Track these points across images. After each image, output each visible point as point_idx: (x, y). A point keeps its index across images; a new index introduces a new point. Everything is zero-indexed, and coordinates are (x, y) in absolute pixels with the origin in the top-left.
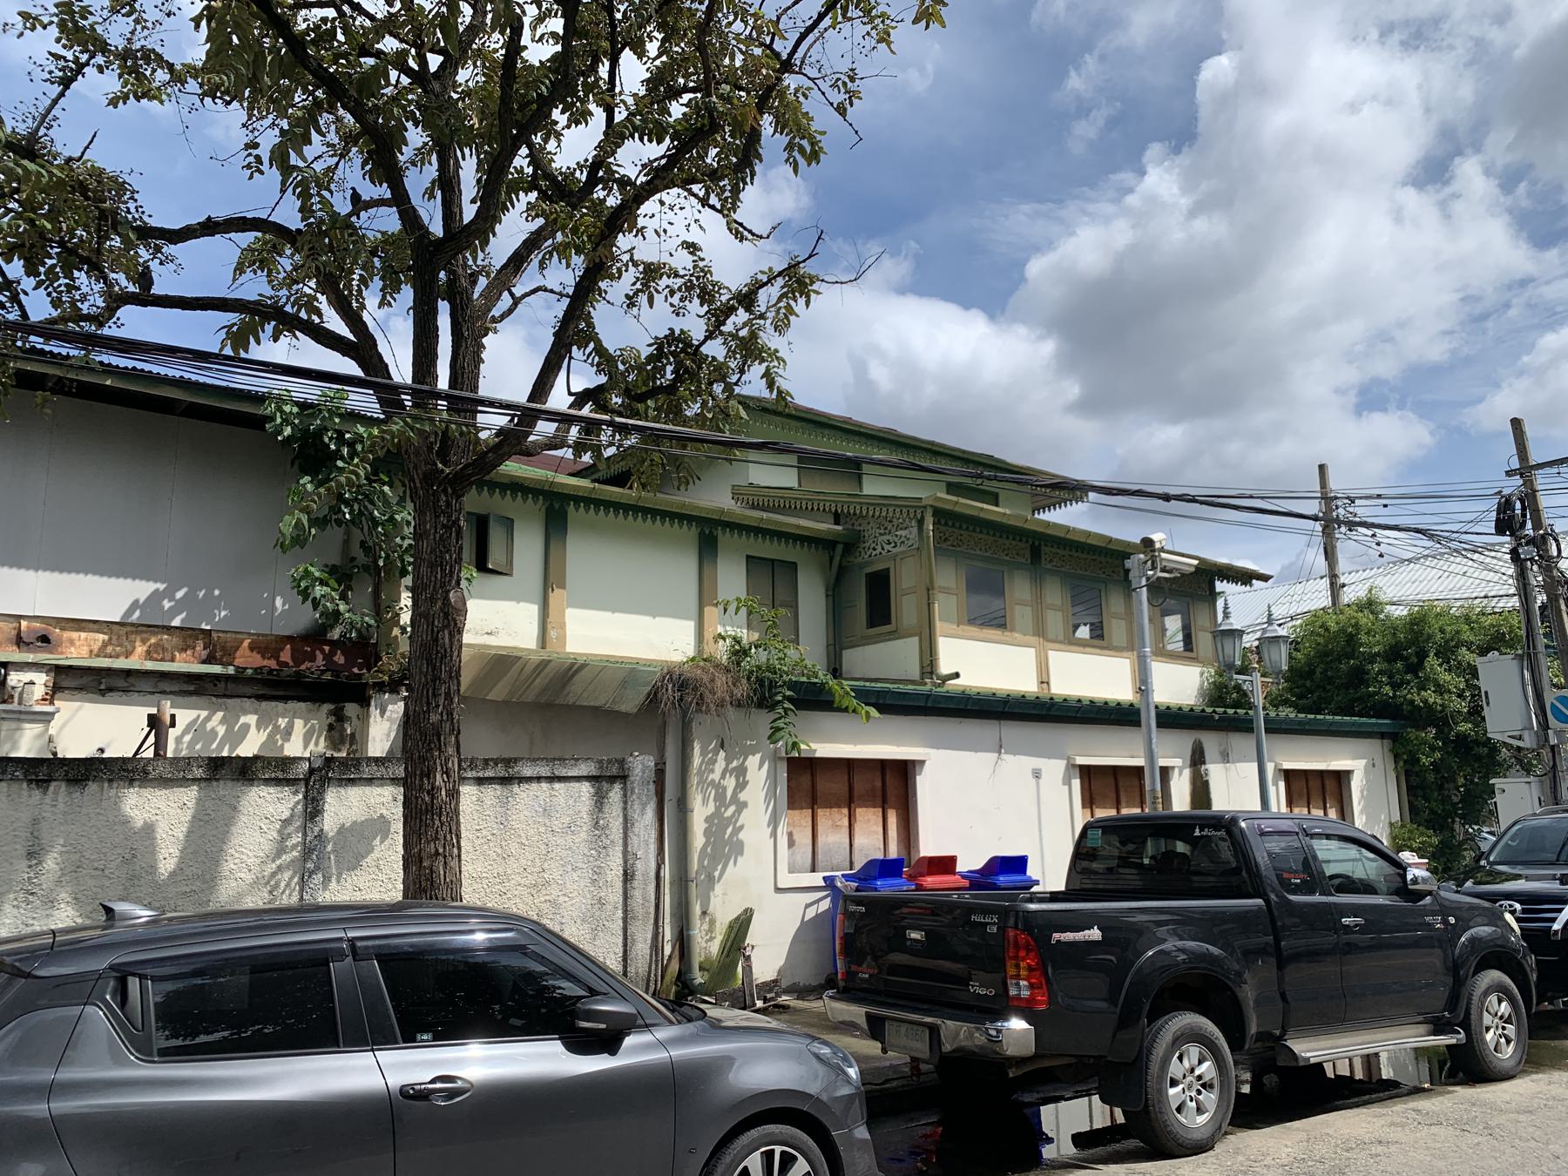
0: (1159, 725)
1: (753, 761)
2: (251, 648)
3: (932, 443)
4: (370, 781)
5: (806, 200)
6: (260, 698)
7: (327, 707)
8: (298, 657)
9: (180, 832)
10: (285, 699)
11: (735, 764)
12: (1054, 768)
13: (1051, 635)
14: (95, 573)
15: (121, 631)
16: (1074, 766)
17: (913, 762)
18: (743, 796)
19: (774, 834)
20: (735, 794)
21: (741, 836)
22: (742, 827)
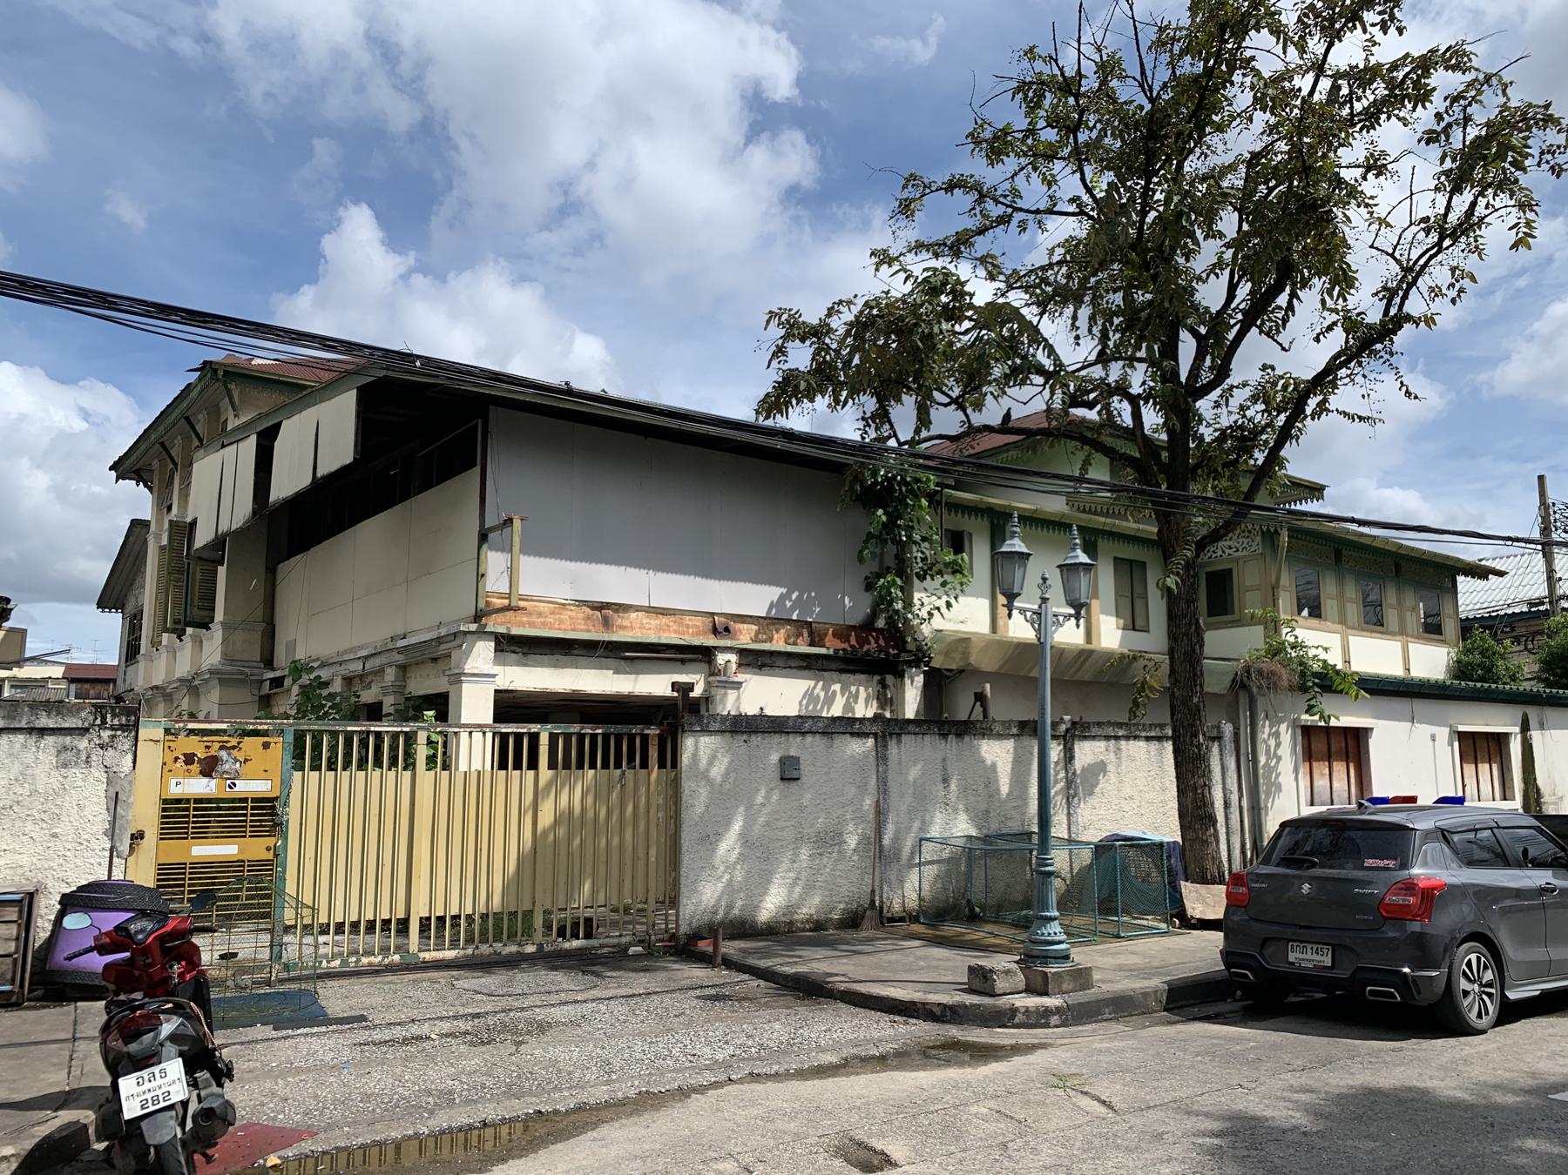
1: (1283, 727)
2: (834, 635)
4: (1094, 738)
5: (811, 165)
6: (842, 671)
7: (877, 678)
8: (863, 641)
9: (1008, 768)
10: (853, 672)
12: (1443, 733)
13: (1350, 623)
14: (697, 574)
15: (768, 623)
19: (1296, 779)
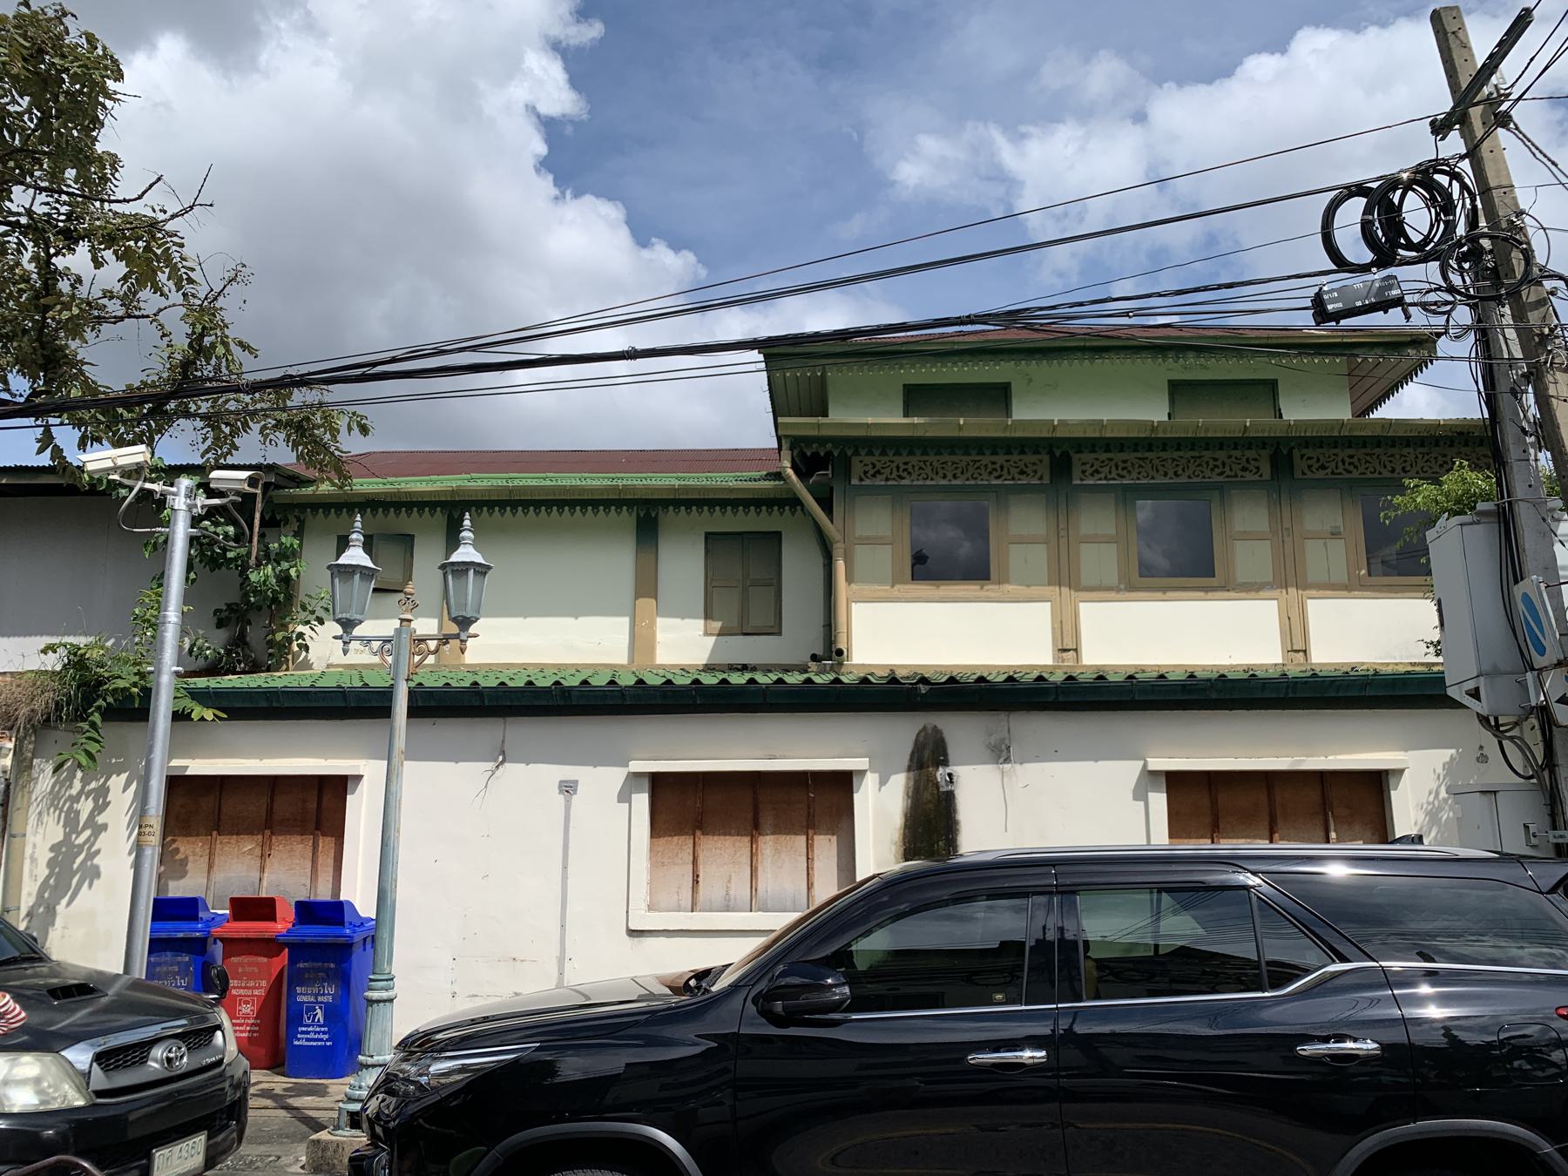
0: (414, 712)
1: (116, 782)
3: (1010, 317)
11: (93, 785)
16: (1154, 774)
17: (1387, 772)
18: (100, 819)
20: (92, 816)
21: (96, 861)
22: (98, 852)
